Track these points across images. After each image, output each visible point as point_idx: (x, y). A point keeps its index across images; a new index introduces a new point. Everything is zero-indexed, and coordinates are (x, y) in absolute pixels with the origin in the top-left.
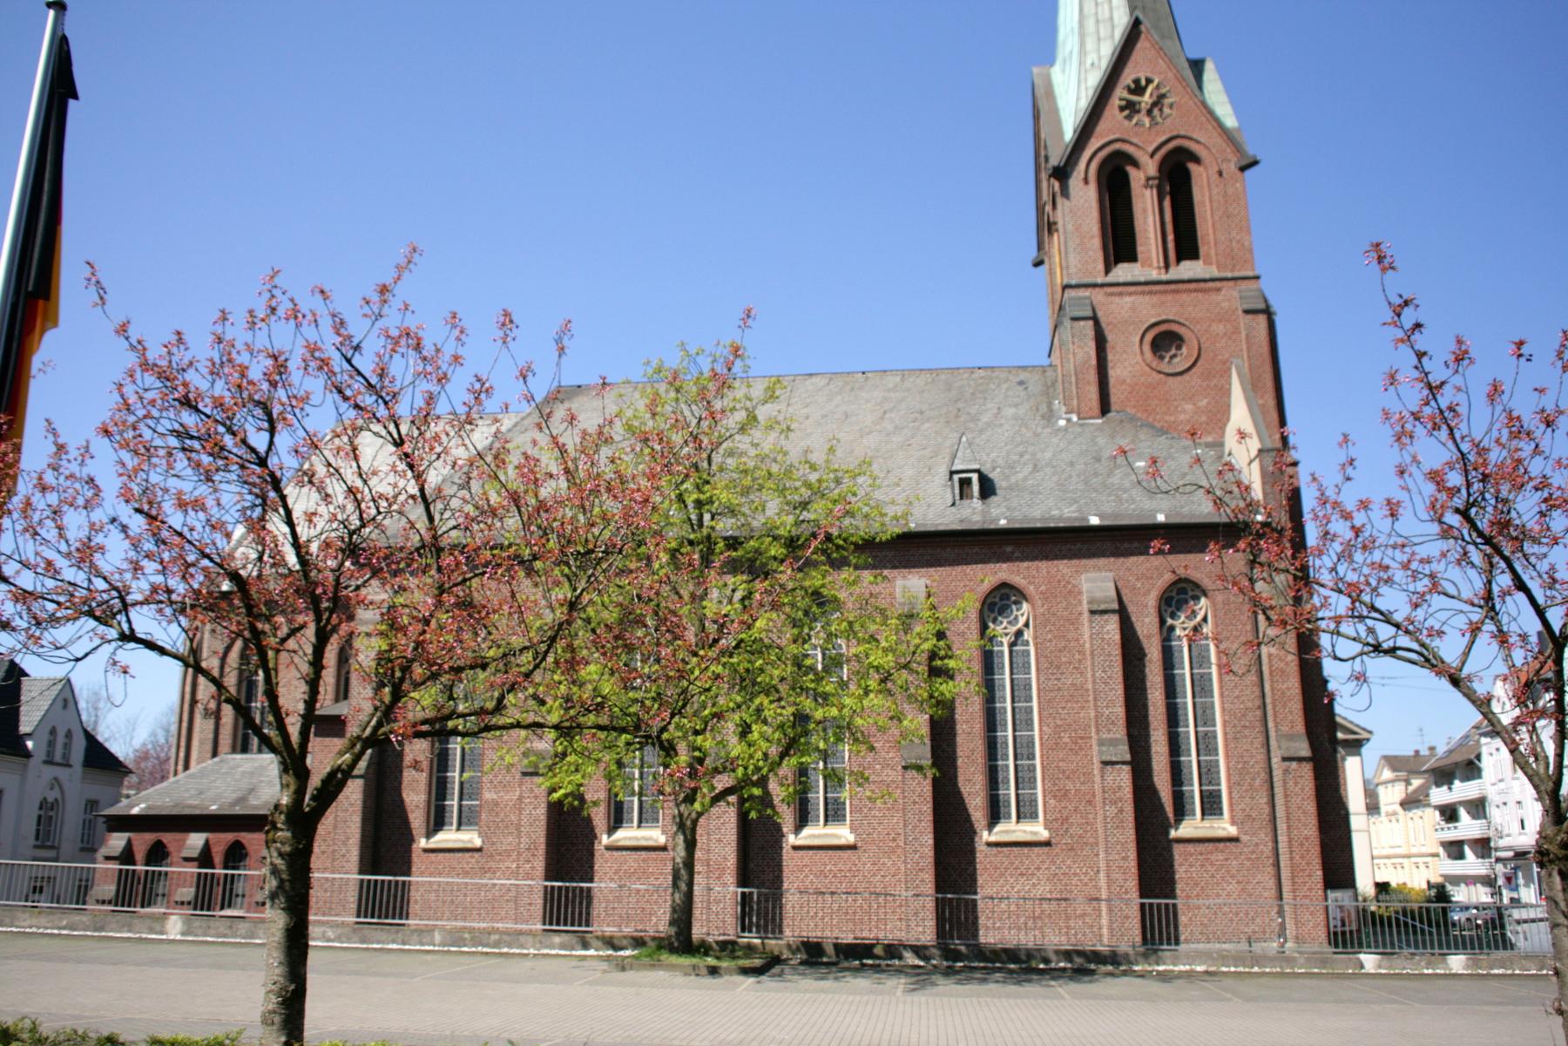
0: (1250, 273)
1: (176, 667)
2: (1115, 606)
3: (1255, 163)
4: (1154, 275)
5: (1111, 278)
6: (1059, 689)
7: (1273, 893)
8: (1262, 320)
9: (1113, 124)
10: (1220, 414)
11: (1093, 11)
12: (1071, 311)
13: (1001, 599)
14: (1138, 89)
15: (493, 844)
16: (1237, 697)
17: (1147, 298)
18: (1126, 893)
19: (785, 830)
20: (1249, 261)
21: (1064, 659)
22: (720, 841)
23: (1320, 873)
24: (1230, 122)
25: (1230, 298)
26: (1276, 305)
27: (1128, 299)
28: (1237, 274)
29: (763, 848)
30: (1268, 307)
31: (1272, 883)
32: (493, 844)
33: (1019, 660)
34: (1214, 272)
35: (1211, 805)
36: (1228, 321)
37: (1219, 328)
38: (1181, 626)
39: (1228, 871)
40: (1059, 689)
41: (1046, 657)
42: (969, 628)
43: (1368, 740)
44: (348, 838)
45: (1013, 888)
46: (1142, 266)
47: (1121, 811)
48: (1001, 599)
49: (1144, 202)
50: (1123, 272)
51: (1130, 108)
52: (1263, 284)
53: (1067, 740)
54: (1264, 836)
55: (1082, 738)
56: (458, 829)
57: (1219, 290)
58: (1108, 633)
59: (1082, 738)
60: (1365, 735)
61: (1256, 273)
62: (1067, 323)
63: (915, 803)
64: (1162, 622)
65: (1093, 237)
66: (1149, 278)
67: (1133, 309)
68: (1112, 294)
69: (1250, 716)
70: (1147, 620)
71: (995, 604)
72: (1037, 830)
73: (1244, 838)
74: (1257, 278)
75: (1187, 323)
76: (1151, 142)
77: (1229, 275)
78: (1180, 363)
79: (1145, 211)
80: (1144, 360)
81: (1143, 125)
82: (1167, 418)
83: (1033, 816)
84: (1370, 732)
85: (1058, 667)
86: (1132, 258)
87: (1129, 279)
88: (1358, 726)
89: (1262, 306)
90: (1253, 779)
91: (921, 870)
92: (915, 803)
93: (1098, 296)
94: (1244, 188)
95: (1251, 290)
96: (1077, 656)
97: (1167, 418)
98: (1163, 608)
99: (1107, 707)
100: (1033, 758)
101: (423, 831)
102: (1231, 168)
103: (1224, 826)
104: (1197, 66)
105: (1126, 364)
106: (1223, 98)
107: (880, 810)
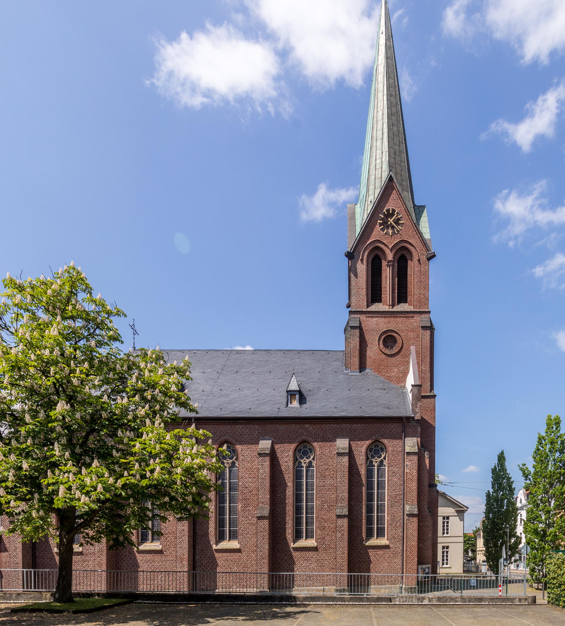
0: (427, 310)
1: (457, 517)
2: (347, 451)
3: (434, 256)
4: (386, 308)
5: (369, 309)
6: (324, 486)
7: (400, 566)
8: (428, 332)
9: (377, 233)
10: (406, 373)
11: (374, 173)
12: (352, 324)
13: (304, 448)
14: (390, 214)
15: (88, 550)
16: (394, 490)
17: (383, 319)
18: (343, 567)
19: (212, 543)
20: (426, 304)
21: (327, 474)
22: (181, 547)
23: (416, 559)
24: (427, 236)
25: (418, 321)
26: (435, 326)
27: (375, 319)
28: (421, 310)
29: (202, 550)
30: (432, 325)
31: (400, 562)
32: (88, 550)
33: (310, 474)
34: (411, 308)
35: (381, 533)
36: (415, 332)
37: (411, 335)
38: (376, 462)
39: (384, 558)
40: (324, 486)
41: (320, 472)
42: (289, 460)
43: (467, 510)
44: (16, 548)
45: (302, 565)
46: (383, 305)
47: (343, 535)
48: (304, 448)
49: (386, 273)
50: (376, 307)
51: (385, 224)
52: (431, 315)
53: (326, 507)
54: (399, 545)
55: (332, 506)
56: (152, 542)
57: (413, 317)
58: (344, 462)
59: (332, 506)
60: (466, 509)
61: (429, 310)
62: (349, 329)
63: (261, 532)
64: (367, 458)
65: (363, 289)
66: (385, 310)
67: (377, 324)
68: (369, 317)
69: (398, 498)
70: (361, 458)
71: (301, 450)
72: (311, 543)
73: (391, 546)
74: (429, 312)
75: (398, 332)
76: (391, 243)
77: (418, 310)
78: (395, 350)
79: (386, 277)
80: (379, 348)
81: (389, 234)
82: (387, 374)
83: (312, 537)
84: (468, 508)
85: (324, 477)
86: (380, 301)
87: (377, 310)
88: (463, 505)
89: (429, 325)
90: (397, 522)
91: (263, 559)
92: (261, 532)
93: (363, 317)
94: (428, 269)
95: (426, 318)
96: (332, 472)
97: (387, 374)
98: (369, 452)
99: (341, 493)
100: (314, 514)
101: (291, 539)
102: (424, 258)
103: (384, 541)
104: (419, 210)
105: (372, 349)
106: (427, 225)
107: (250, 534)
